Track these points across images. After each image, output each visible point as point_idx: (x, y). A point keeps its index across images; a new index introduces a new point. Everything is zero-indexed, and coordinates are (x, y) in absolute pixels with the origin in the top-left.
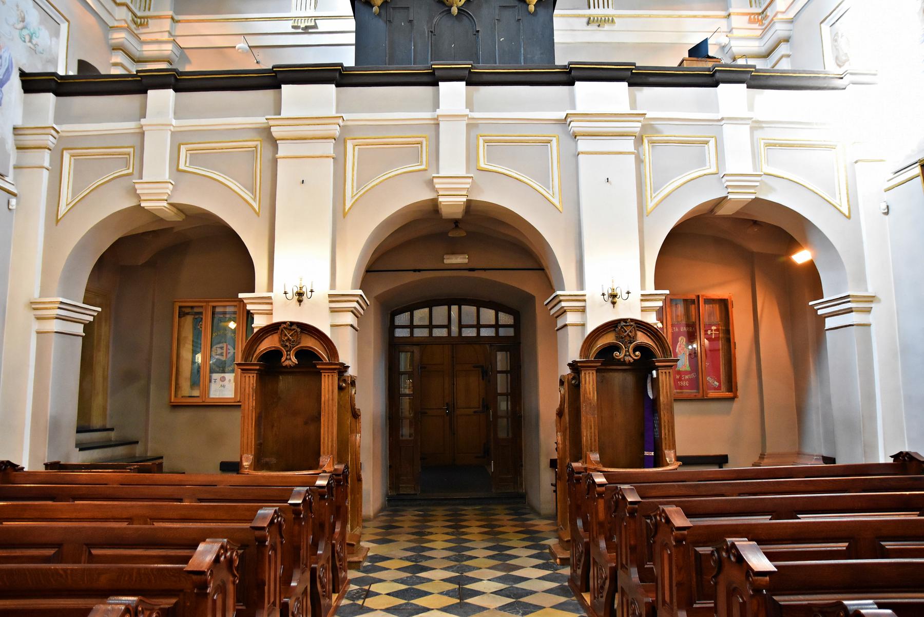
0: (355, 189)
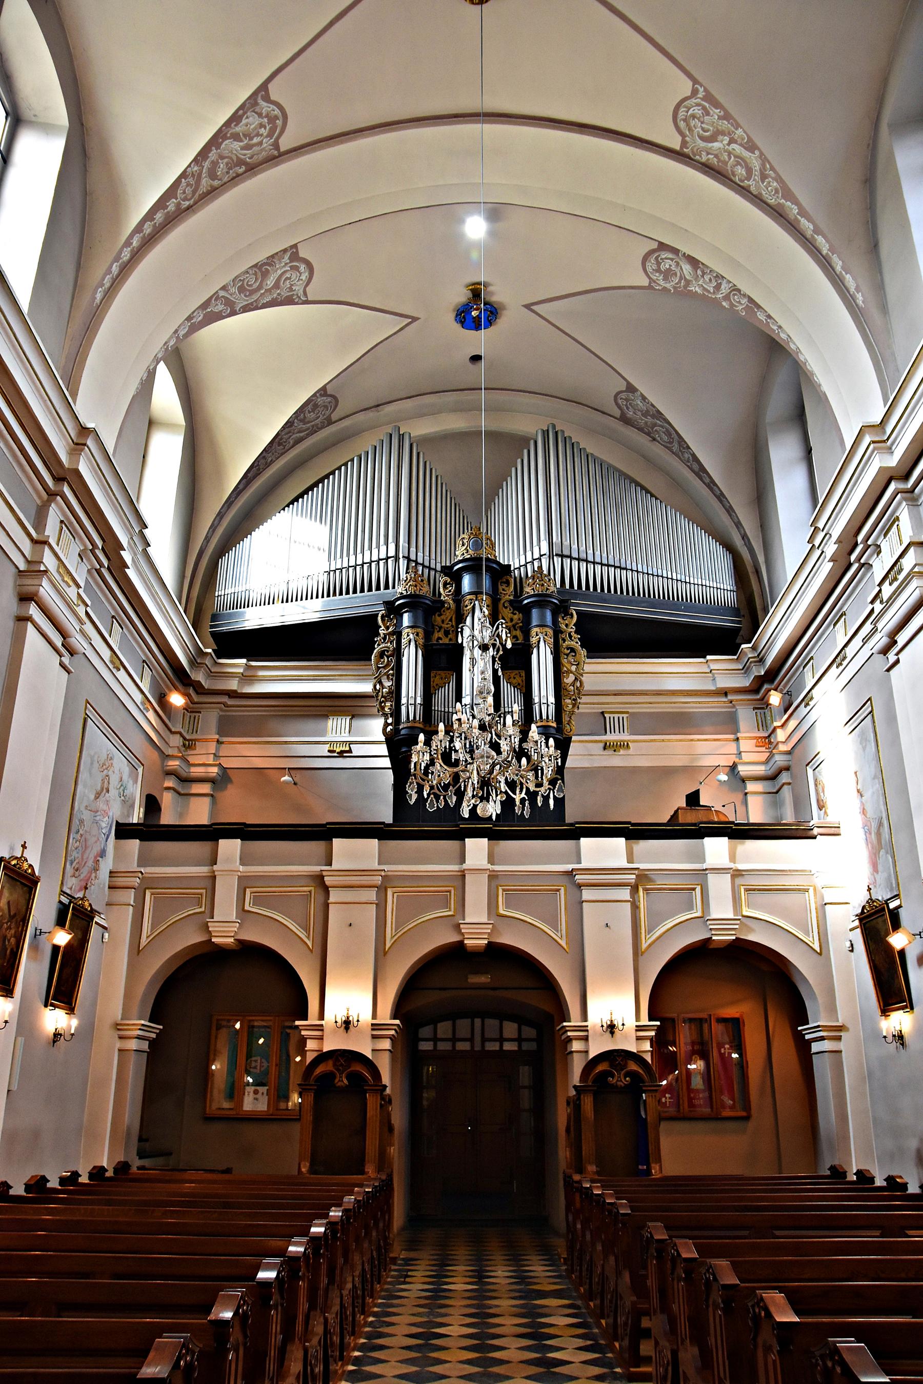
0: (394, 931)
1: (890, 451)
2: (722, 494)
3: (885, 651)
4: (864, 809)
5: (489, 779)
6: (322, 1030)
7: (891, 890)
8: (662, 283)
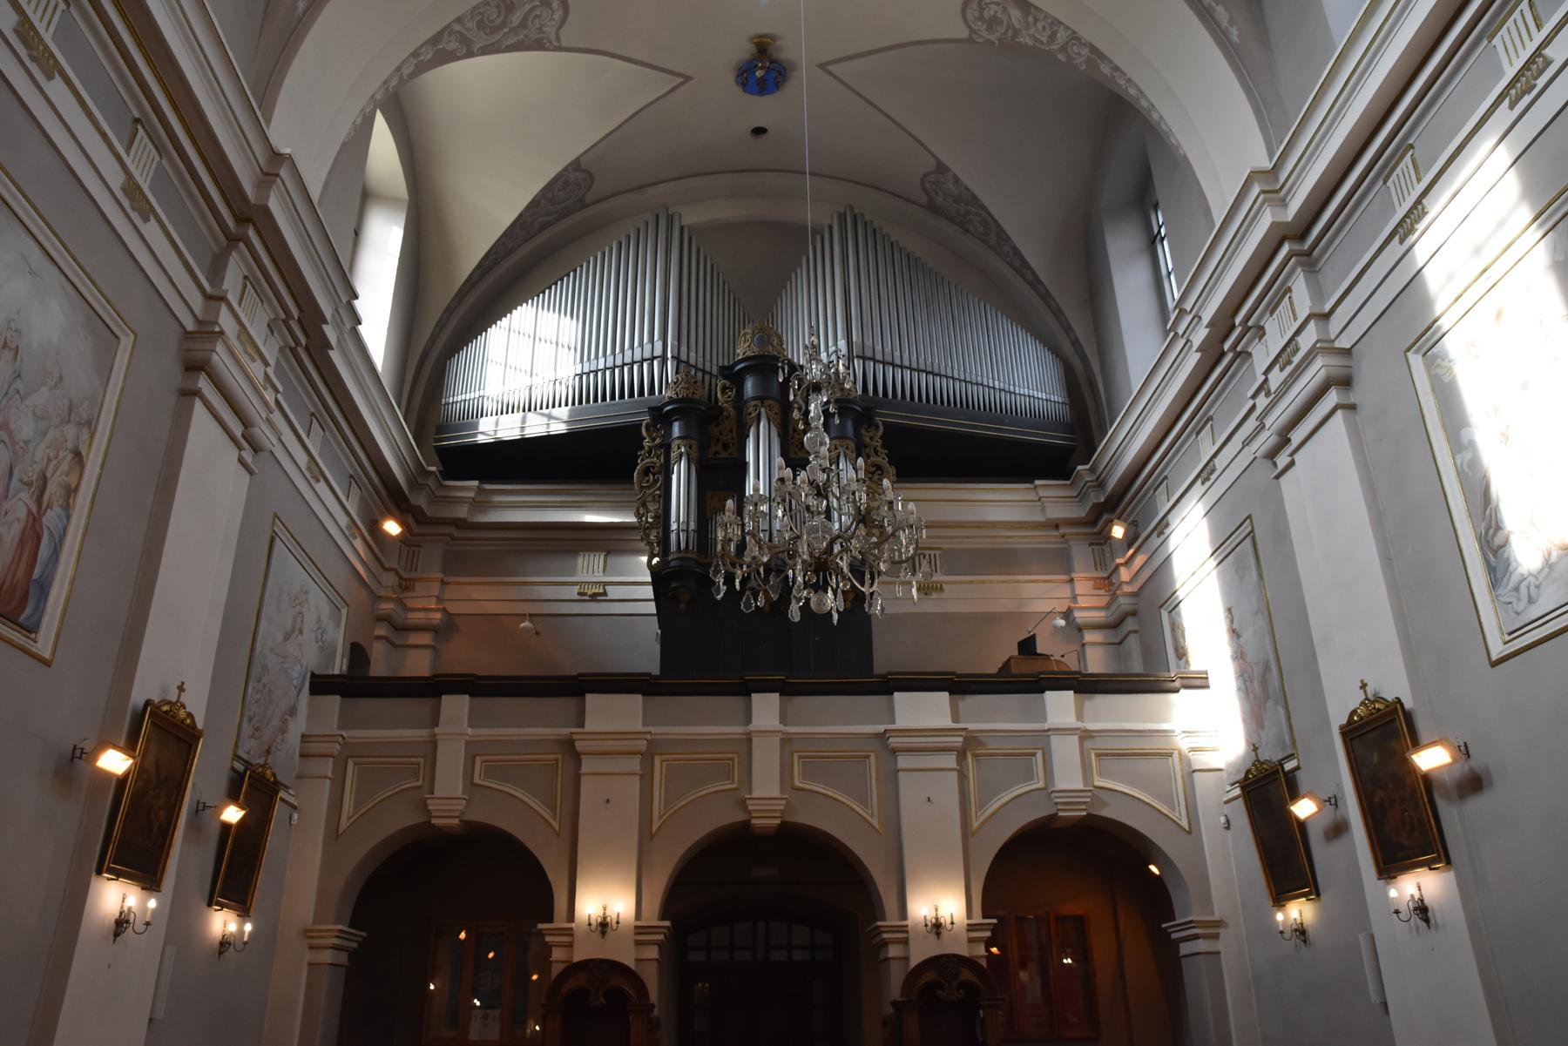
0: (662, 809)
1: (1284, 203)
2: (1048, 293)
3: (1272, 455)
4: (1242, 653)
5: (826, 561)
6: (572, 935)
7: (1284, 749)
8: (984, 34)
